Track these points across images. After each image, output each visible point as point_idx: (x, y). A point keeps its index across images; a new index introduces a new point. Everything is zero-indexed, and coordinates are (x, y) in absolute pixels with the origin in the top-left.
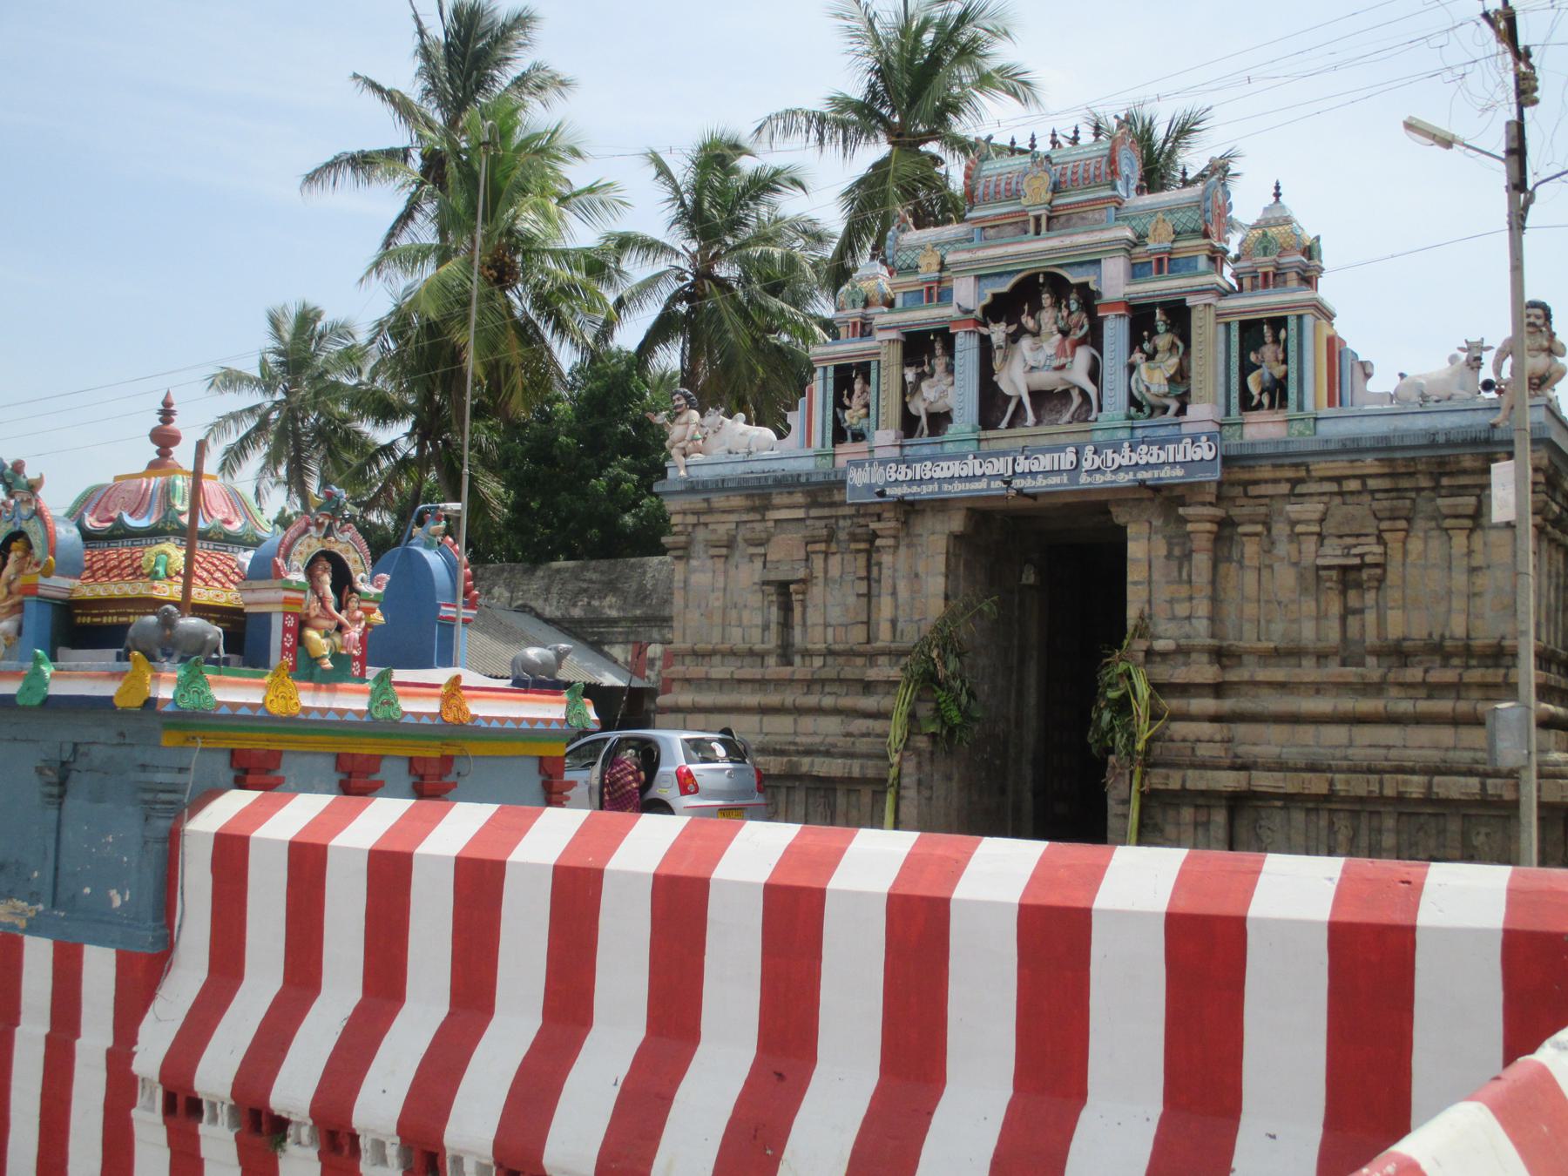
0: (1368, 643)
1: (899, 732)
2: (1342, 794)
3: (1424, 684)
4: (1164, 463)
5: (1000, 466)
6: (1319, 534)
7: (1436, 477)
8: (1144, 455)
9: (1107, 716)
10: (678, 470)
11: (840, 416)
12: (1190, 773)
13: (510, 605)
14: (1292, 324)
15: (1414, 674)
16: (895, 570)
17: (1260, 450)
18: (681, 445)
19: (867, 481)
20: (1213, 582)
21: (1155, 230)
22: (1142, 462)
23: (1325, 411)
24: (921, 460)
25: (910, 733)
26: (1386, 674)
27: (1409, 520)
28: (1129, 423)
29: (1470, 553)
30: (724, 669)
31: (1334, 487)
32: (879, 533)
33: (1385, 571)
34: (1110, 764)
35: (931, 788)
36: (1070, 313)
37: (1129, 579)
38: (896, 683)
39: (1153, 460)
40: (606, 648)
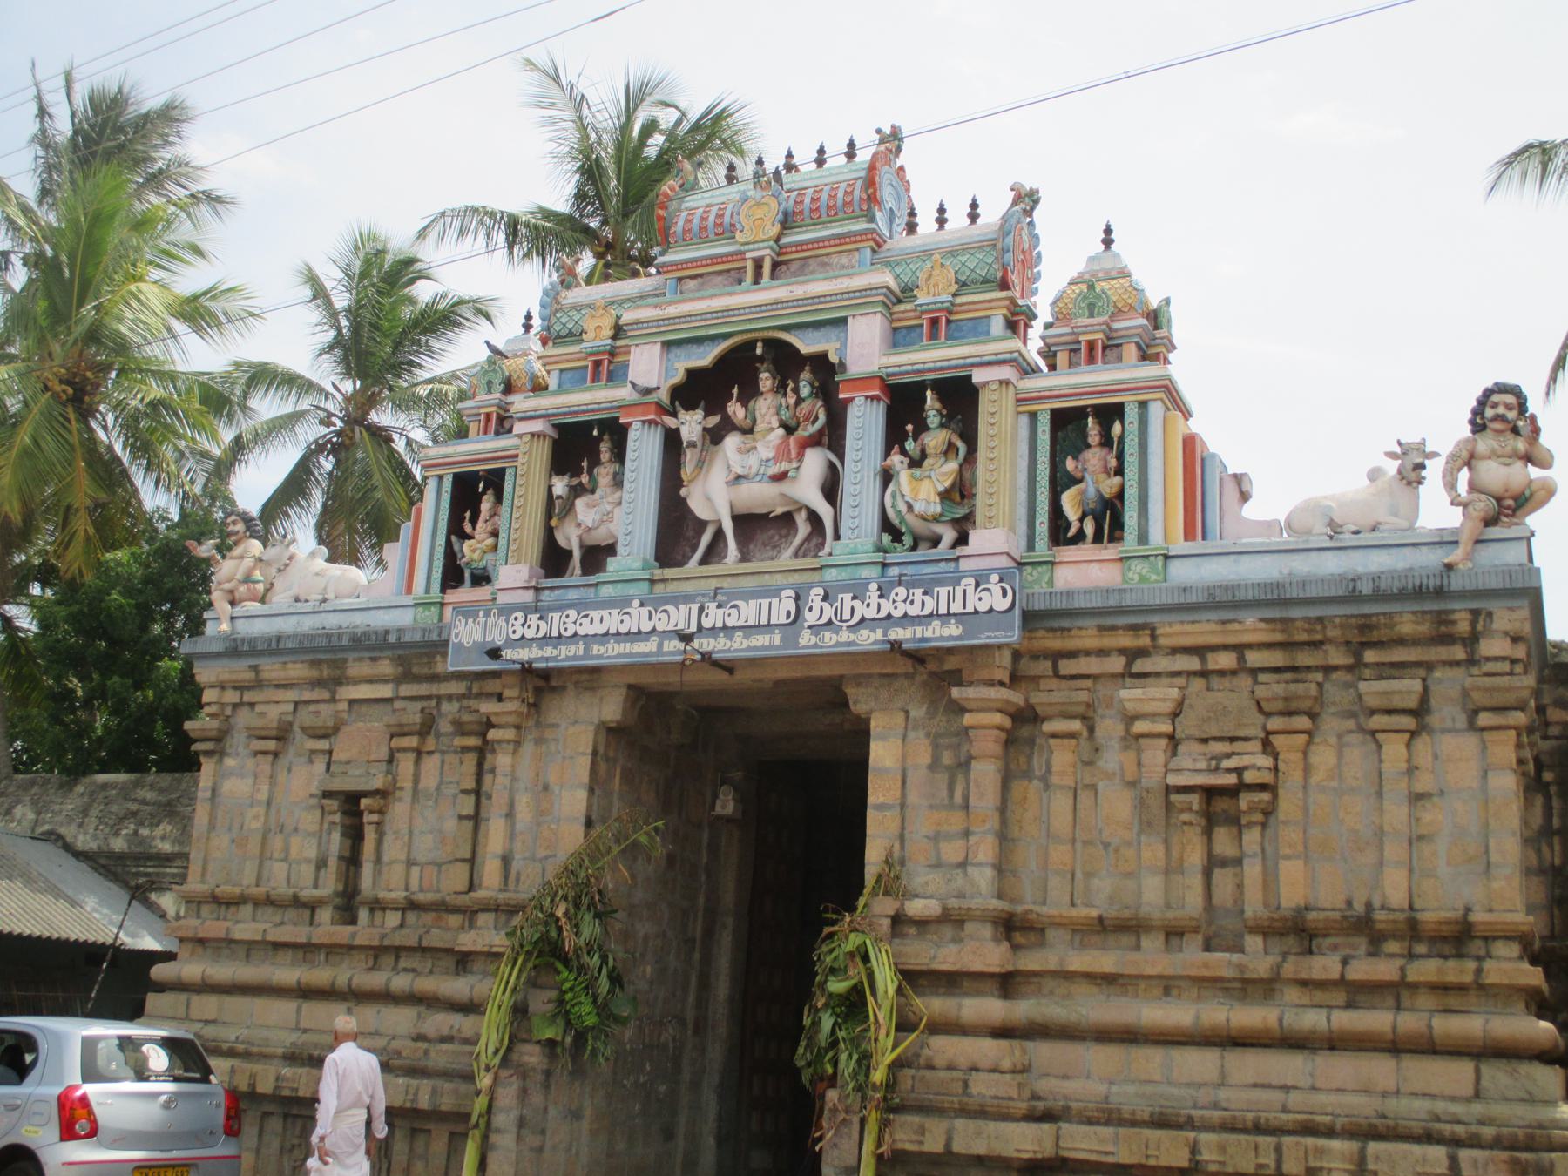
0: (1249, 913)
1: (494, 1037)
2: (1213, 1168)
3: (1342, 982)
4: (931, 615)
5: (679, 617)
6: (1171, 737)
7: (1357, 649)
8: (900, 603)
9: (827, 1022)
10: (219, 624)
11: (456, 547)
12: (960, 1123)
13: (33, 830)
14: (1131, 414)
15: (1325, 965)
16: (514, 779)
17: (1080, 603)
18: (227, 586)
19: (479, 638)
20: (1003, 809)
21: (930, 277)
22: (897, 613)
23: (1180, 546)
24: (561, 607)
25: (513, 1039)
26: (1279, 966)
27: (1313, 716)
28: (879, 557)
29: (1411, 770)
30: (254, 925)
31: (1193, 663)
32: (494, 719)
33: (1275, 796)
34: (829, 1105)
35: (543, 1132)
36: (799, 401)
37: (871, 799)
38: (498, 955)
39: (914, 611)
40: (153, 896)
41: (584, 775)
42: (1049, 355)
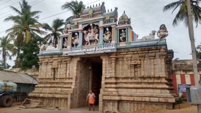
5: (84, 50)
23: (131, 42)
29: (154, 62)
41: (76, 65)
42: (119, 24)
